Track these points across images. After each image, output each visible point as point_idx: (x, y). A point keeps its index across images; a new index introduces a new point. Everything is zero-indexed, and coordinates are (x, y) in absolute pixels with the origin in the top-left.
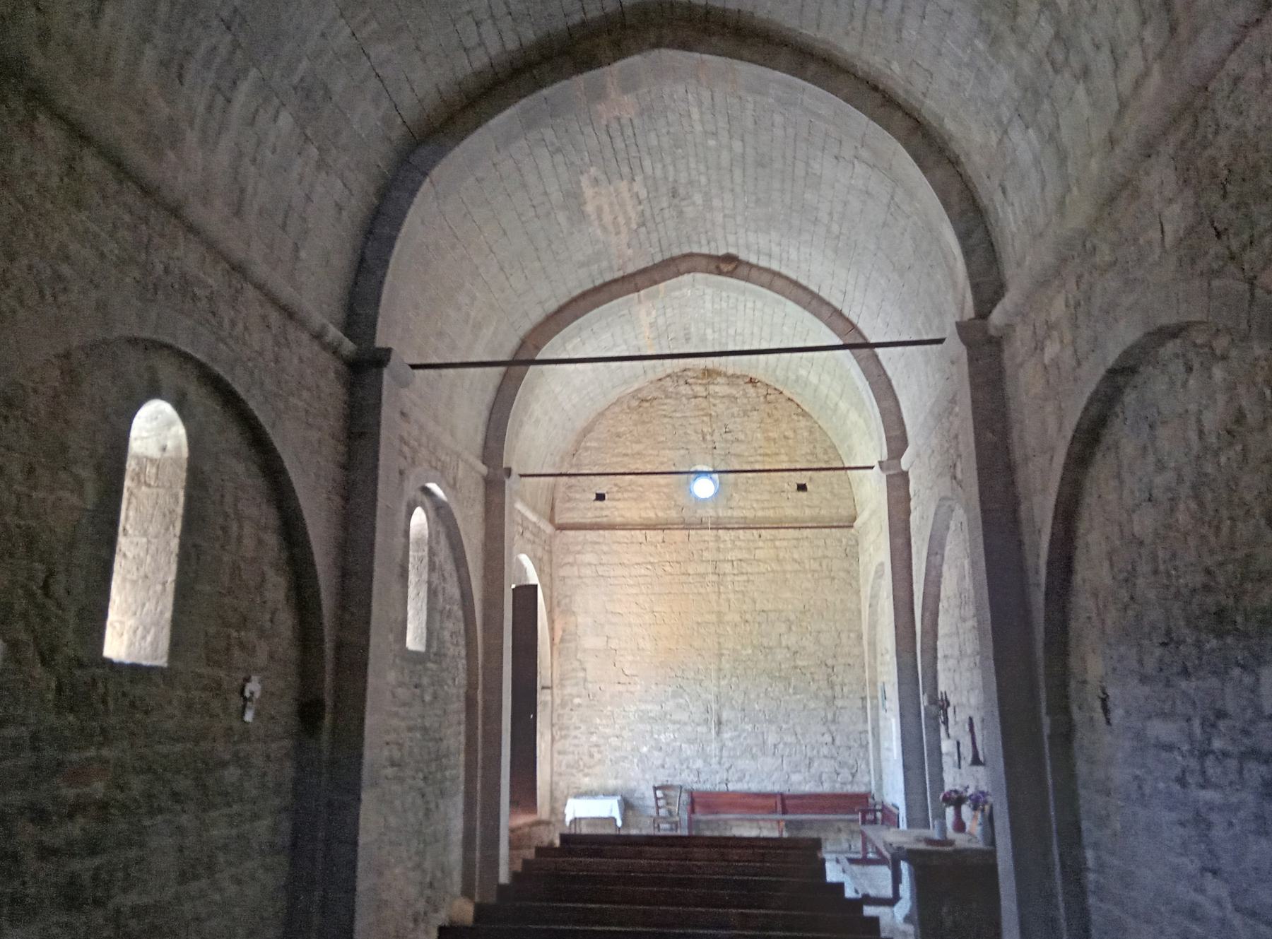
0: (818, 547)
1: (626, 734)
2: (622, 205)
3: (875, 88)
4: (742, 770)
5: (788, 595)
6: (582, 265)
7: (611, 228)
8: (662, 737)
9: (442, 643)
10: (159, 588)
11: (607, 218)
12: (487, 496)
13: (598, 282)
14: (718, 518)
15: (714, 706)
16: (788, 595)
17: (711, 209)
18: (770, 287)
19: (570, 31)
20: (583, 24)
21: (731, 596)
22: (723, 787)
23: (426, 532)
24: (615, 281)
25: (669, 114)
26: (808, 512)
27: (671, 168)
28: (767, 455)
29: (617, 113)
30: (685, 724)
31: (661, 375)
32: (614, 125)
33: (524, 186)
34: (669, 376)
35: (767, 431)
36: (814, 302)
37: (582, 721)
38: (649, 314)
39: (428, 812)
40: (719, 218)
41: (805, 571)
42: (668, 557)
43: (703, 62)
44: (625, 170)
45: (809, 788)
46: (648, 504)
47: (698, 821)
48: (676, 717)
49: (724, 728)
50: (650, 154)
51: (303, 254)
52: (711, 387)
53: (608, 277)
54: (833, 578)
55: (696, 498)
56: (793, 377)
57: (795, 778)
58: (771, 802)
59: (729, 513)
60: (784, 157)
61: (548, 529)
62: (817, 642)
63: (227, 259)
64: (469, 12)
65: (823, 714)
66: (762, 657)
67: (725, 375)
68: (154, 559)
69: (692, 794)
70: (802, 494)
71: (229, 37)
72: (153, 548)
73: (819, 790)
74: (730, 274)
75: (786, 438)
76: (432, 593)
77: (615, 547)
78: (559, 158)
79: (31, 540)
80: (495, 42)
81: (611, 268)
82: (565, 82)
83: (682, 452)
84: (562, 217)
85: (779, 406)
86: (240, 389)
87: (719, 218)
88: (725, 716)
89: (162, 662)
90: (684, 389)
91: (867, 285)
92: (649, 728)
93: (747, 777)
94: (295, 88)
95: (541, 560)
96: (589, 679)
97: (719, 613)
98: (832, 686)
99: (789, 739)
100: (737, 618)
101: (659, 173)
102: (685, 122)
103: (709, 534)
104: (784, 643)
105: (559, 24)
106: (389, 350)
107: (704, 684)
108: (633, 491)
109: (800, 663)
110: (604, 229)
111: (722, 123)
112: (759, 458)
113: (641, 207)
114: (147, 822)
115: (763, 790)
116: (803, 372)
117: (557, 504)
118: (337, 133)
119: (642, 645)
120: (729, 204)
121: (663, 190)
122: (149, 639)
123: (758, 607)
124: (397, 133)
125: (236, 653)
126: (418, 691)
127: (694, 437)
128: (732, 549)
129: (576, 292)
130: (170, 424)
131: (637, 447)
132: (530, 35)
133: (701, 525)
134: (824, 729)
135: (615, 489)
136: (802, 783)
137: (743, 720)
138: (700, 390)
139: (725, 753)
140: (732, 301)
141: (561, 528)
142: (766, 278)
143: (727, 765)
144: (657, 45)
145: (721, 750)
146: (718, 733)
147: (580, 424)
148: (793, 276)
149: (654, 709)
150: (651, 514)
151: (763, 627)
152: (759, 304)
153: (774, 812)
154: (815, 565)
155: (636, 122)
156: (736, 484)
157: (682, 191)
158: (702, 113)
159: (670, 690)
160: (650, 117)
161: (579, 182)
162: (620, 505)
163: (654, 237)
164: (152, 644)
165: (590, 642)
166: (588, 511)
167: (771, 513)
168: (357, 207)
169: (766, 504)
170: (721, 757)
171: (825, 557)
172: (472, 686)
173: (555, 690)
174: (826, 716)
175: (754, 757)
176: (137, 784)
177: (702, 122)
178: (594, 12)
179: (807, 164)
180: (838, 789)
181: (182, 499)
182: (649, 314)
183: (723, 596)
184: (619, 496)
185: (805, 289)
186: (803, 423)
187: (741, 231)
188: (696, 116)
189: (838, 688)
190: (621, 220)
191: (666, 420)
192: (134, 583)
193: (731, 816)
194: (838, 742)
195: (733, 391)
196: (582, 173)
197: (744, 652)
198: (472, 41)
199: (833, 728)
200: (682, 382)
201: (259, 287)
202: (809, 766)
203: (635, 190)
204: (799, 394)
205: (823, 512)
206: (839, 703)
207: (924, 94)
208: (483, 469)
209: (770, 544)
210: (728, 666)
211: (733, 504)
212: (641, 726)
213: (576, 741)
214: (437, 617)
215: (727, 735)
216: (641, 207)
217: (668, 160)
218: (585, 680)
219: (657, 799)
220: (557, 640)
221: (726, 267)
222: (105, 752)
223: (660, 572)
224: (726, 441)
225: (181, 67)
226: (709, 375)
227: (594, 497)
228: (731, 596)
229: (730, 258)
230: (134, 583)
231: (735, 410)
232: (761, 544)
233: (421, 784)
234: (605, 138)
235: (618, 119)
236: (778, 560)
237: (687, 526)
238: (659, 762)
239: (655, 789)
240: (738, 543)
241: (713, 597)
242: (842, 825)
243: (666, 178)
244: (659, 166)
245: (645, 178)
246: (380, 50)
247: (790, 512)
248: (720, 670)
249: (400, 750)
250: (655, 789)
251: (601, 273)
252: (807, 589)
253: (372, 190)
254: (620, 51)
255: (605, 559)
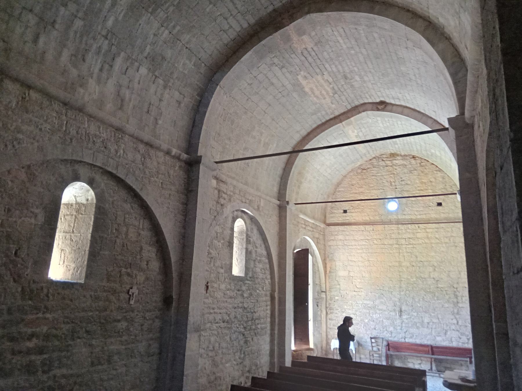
0: (448, 231)
1: (358, 313)
2: (322, 86)
3: (408, 11)
4: (412, 333)
5: (433, 254)
6: (313, 114)
7: (320, 96)
8: (374, 316)
9: (254, 272)
10: (83, 253)
11: (317, 93)
12: (280, 213)
13: (324, 121)
14: (398, 219)
15: (398, 304)
16: (433, 254)
17: (365, 82)
18: (402, 114)
19: (270, 14)
20: (275, 10)
21: (405, 254)
22: (403, 340)
23: (245, 228)
24: (331, 119)
25: (329, 42)
26: (443, 216)
27: (340, 67)
28: (422, 190)
29: (304, 46)
30: (385, 311)
31: (371, 158)
32: (305, 52)
33: (272, 84)
34: (374, 158)
35: (421, 179)
36: (424, 118)
37: (339, 307)
38: (353, 132)
39: (246, 342)
40: (370, 86)
41: (442, 243)
42: (375, 237)
43: (329, 16)
44: (318, 71)
45: (446, 344)
46: (366, 214)
47: (391, 355)
48: (380, 307)
49: (403, 314)
50: (326, 62)
51: (160, 122)
52: (394, 161)
53: (328, 118)
54: (456, 246)
55: (388, 211)
56: (430, 154)
57: (439, 339)
58: (427, 349)
59: (404, 217)
60: (385, 52)
61: (323, 226)
62: (449, 276)
63: (112, 126)
64: (221, 15)
65: (452, 309)
66: (420, 282)
67: (401, 156)
68: (82, 242)
69: (388, 341)
70: (440, 208)
71: (107, 42)
72: (82, 238)
73: (451, 345)
74: (383, 110)
75: (431, 182)
76: (248, 253)
77: (352, 232)
78: (284, 70)
79: (8, 237)
80: (237, 26)
81: (327, 114)
82: (271, 37)
83: (381, 191)
84: (295, 95)
85: (427, 167)
86: (122, 177)
87: (370, 86)
88: (403, 308)
89: (82, 281)
90: (382, 163)
91: (441, 106)
92: (368, 311)
93: (415, 337)
94: (146, 58)
95: (318, 238)
96: (342, 289)
97: (399, 262)
98: (456, 297)
99: (435, 320)
100: (408, 264)
101: (334, 69)
102: (338, 44)
103: (394, 227)
104: (432, 276)
105: (263, 13)
106: (201, 156)
107: (393, 293)
108: (359, 208)
109: (440, 286)
110: (317, 97)
111: (353, 42)
112: (418, 192)
113: (331, 86)
114: (70, 342)
115: (423, 343)
116: (433, 151)
117: (327, 215)
118: (172, 73)
119: (364, 275)
120: (371, 78)
121: (339, 77)
122: (79, 272)
123: (419, 259)
124: (203, 70)
125: (125, 278)
126: (240, 292)
127: (387, 184)
128: (405, 233)
129: (314, 126)
130: (88, 191)
131: (361, 190)
132: (252, 21)
133: (390, 223)
134: (453, 317)
135: (351, 208)
136: (441, 341)
137: (412, 310)
138: (388, 163)
139: (404, 325)
140: (391, 122)
141: (329, 225)
142: (400, 109)
143: (405, 330)
144: (309, 12)
145: (402, 324)
146: (400, 316)
147: (335, 181)
148: (412, 107)
149: (370, 303)
150: (367, 218)
151: (421, 269)
152: (399, 123)
153: (428, 353)
154: (447, 240)
155: (315, 48)
156: (406, 204)
157: (348, 76)
158: (343, 39)
159: (377, 295)
160: (321, 46)
161: (297, 79)
162: (354, 214)
163: (343, 98)
164: (79, 274)
165: (342, 273)
166: (340, 218)
167: (424, 217)
168: (188, 101)
169: (421, 213)
170: (402, 327)
171: (452, 236)
172: (273, 291)
173: (328, 293)
174: (454, 311)
175: (418, 328)
176: (66, 328)
177: (345, 43)
178: (278, 4)
179: (396, 54)
180: (460, 345)
181: (93, 219)
182: (353, 132)
183: (401, 254)
184: (353, 211)
185: (419, 112)
186: (439, 174)
187: (382, 89)
188: (341, 41)
189: (459, 298)
190: (324, 92)
191: (374, 177)
192: (75, 251)
193: (407, 354)
194: (460, 323)
195: (404, 162)
196: (297, 75)
197: (412, 280)
198: (226, 27)
199: (457, 317)
200: (380, 160)
201: (132, 136)
202: (445, 334)
203: (326, 78)
204: (436, 162)
205: (451, 215)
206: (460, 305)
207: (428, 8)
208: (278, 202)
209: (423, 230)
210: (404, 286)
211: (405, 213)
212: (364, 311)
213: (336, 315)
214: (252, 263)
215: (404, 317)
216: (331, 86)
217: (337, 63)
218: (340, 289)
219: (372, 343)
220: (328, 272)
221: (380, 107)
222: (48, 315)
223: (371, 243)
224: (402, 185)
225: (84, 56)
226: (393, 156)
227: (342, 211)
228: (405, 254)
229: (382, 103)
230: (75, 251)
231: (406, 170)
232: (419, 231)
233: (243, 330)
234: (303, 58)
235: (306, 49)
236: (428, 238)
237: (383, 223)
238: (373, 327)
239: (371, 338)
240: (408, 230)
241: (397, 255)
242: (463, 363)
243: (339, 71)
244: (333, 66)
245: (328, 73)
246: (186, 37)
247: (433, 216)
248: (400, 287)
249: (229, 316)
250: (371, 338)
251: (323, 116)
252: (443, 252)
253: (195, 94)
254: (292, 19)
255: (347, 238)
